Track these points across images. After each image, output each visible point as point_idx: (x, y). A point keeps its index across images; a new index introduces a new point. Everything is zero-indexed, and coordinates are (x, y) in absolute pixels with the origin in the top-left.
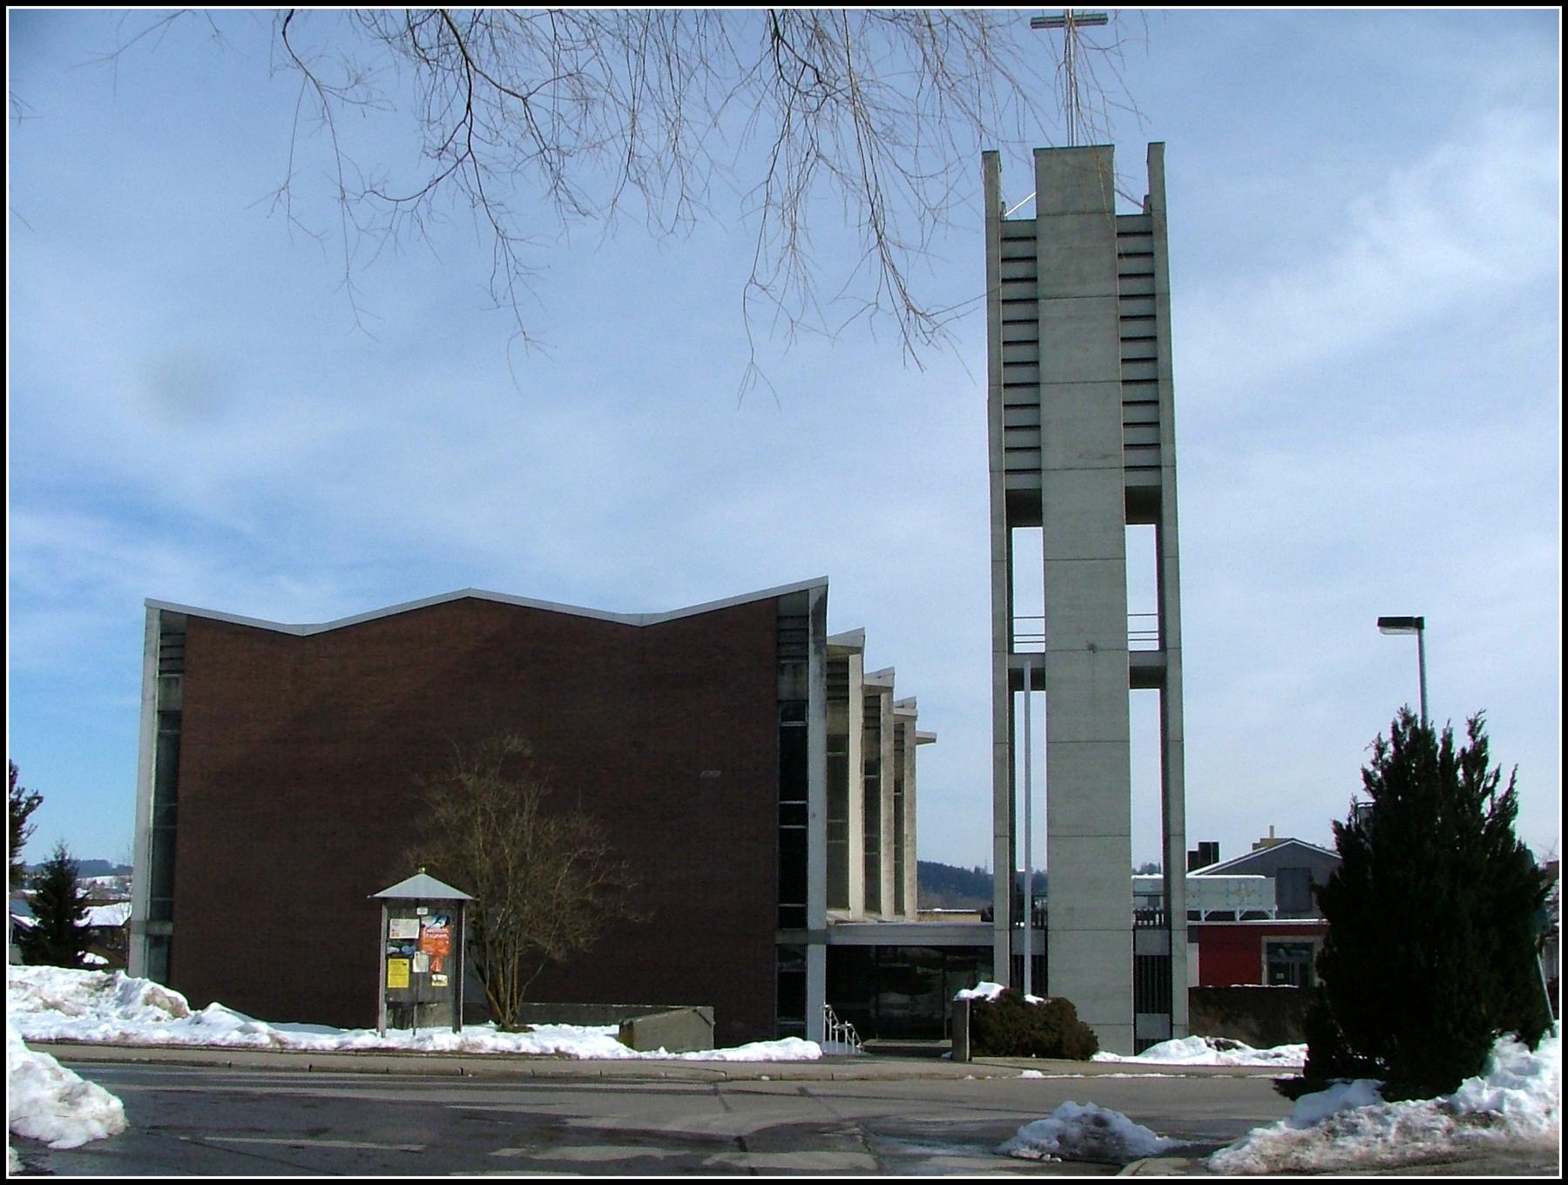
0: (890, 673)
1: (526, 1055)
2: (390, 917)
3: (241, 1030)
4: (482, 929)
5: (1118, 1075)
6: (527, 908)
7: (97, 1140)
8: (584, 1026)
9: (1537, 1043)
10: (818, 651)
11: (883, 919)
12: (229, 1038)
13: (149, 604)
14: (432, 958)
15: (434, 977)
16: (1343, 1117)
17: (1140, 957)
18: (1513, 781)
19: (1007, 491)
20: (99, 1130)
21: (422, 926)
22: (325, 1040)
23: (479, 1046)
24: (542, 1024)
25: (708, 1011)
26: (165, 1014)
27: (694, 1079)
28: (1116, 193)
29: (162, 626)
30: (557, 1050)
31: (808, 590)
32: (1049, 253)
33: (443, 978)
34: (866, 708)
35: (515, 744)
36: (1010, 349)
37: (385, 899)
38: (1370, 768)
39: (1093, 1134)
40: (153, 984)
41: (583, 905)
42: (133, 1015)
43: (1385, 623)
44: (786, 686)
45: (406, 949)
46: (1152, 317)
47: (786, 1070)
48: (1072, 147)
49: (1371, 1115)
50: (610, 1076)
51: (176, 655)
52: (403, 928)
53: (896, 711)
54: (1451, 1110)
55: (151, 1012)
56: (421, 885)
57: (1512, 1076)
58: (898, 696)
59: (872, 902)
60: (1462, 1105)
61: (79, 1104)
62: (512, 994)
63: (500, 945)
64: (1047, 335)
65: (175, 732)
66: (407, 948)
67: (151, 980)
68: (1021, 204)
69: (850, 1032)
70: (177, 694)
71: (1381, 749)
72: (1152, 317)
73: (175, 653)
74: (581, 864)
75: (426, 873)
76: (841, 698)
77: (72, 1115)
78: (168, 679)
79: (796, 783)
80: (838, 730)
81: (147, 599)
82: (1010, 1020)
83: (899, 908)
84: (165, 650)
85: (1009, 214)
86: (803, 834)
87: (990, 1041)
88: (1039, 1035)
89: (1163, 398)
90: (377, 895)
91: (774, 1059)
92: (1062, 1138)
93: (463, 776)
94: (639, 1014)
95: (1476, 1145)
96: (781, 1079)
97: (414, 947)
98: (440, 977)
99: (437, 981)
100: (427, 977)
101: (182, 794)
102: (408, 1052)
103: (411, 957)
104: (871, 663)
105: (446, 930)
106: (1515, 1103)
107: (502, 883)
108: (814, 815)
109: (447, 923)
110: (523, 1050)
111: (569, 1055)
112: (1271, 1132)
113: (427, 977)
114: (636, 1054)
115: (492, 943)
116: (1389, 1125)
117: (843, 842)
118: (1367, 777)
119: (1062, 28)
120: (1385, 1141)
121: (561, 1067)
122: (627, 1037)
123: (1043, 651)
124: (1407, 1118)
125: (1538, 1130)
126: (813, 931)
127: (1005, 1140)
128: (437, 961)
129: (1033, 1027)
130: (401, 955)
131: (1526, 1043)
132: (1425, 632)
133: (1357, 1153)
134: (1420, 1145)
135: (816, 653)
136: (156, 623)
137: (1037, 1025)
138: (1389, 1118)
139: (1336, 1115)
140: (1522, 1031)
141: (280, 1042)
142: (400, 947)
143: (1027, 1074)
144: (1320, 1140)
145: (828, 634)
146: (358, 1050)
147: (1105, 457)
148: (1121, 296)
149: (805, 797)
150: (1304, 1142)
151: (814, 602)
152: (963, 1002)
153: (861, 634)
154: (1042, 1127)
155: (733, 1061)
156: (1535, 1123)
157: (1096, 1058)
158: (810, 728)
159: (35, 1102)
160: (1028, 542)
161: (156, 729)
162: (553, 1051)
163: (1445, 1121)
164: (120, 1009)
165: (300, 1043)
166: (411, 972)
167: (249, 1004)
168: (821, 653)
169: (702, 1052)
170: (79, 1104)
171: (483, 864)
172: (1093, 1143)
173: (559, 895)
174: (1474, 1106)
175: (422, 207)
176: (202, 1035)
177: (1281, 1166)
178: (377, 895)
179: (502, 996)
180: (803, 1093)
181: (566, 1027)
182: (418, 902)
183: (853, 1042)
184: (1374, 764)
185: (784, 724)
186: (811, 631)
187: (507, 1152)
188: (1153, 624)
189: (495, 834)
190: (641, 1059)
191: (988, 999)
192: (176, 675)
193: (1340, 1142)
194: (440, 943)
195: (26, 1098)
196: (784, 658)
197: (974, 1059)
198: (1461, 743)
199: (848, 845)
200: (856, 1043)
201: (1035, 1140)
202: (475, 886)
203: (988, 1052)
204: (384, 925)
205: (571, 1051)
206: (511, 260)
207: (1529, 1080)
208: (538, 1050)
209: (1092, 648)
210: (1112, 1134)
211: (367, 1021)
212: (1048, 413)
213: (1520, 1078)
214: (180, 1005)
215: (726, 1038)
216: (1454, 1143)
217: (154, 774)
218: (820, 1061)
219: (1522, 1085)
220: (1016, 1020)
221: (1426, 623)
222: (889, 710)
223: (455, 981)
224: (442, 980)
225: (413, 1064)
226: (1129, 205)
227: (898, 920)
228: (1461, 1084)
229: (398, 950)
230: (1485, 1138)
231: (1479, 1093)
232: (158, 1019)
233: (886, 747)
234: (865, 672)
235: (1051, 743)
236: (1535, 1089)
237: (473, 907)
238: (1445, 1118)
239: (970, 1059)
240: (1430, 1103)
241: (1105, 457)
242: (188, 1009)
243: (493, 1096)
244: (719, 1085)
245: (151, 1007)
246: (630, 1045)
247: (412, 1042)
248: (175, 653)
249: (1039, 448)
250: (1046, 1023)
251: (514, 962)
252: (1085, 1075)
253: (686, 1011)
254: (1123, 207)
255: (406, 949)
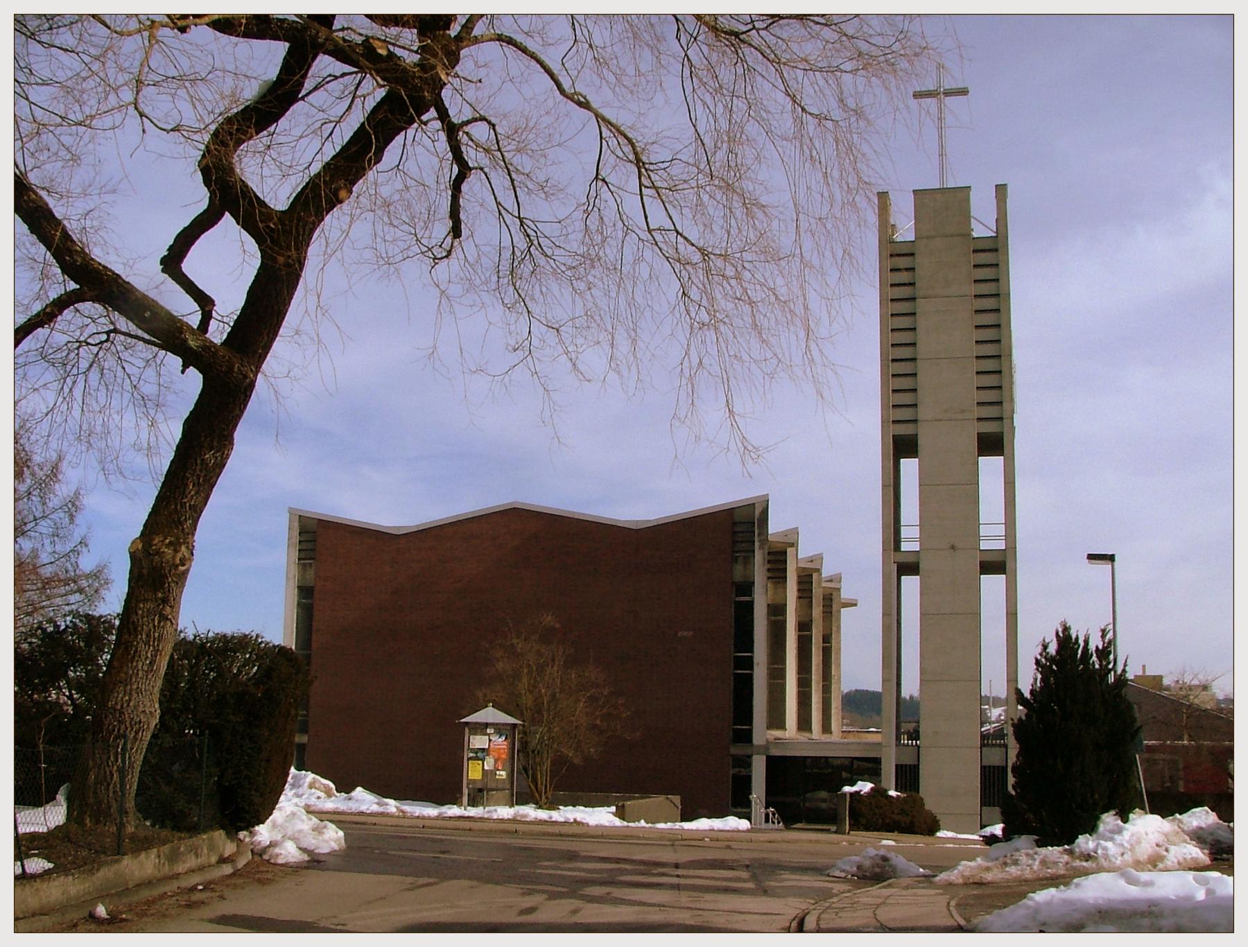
0: (820, 558)
1: (556, 823)
2: (470, 734)
3: (378, 804)
4: (527, 742)
5: (949, 845)
6: (555, 730)
7: (335, 851)
8: (593, 807)
9: (1128, 817)
10: (761, 547)
11: (813, 738)
12: (371, 808)
13: (292, 511)
14: (496, 761)
15: (498, 772)
16: (1012, 856)
17: (985, 767)
18: (1125, 665)
19: (893, 436)
20: (335, 846)
21: (490, 740)
22: (431, 811)
23: (526, 816)
24: (565, 806)
25: (677, 799)
26: (322, 795)
27: (661, 838)
28: (972, 220)
29: (300, 526)
30: (575, 820)
31: (754, 504)
32: (924, 265)
33: (503, 773)
34: (799, 583)
35: (549, 619)
36: (896, 334)
37: (467, 723)
38: (1039, 657)
39: (878, 866)
40: (314, 775)
41: (595, 727)
42: (302, 795)
43: (1091, 557)
44: (738, 572)
45: (480, 754)
46: (998, 311)
47: (721, 835)
48: (944, 188)
49: (1027, 855)
50: (607, 835)
51: (310, 547)
52: (478, 742)
53: (824, 585)
54: (1070, 852)
55: (314, 793)
56: (489, 714)
57: (1108, 834)
58: (826, 573)
59: (804, 723)
60: (1077, 850)
61: (323, 833)
62: (546, 786)
63: (538, 753)
64: (922, 323)
65: (309, 601)
66: (481, 754)
67: (313, 773)
68: (905, 231)
69: (774, 814)
70: (311, 574)
71: (1045, 647)
72: (998, 311)
73: (310, 546)
74: (593, 699)
75: (493, 706)
76: (782, 578)
77: (321, 838)
78: (304, 565)
79: (744, 639)
80: (779, 601)
81: (290, 508)
82: (877, 807)
83: (826, 728)
84: (303, 543)
85: (898, 237)
86: (750, 677)
87: (863, 821)
88: (897, 817)
89: (1005, 370)
90: (462, 720)
91: (716, 829)
92: (859, 867)
93: (515, 641)
94: (630, 799)
95: (1079, 870)
96: (717, 840)
97: (485, 754)
98: (502, 773)
99: (500, 775)
100: (493, 772)
101: (314, 645)
102: (481, 819)
103: (483, 760)
104: (805, 550)
105: (505, 743)
106: (1105, 849)
107: (539, 712)
108: (758, 664)
109: (506, 738)
110: (553, 819)
111: (583, 823)
112: (973, 864)
113: (493, 772)
114: (625, 823)
115: (533, 752)
116: (1035, 860)
117: (807, 676)
118: (1038, 662)
119: (946, 87)
120: (1031, 869)
121: (577, 830)
122: (621, 814)
123: (918, 549)
124: (1046, 856)
125: (1115, 863)
126: (758, 746)
127: (827, 869)
128: (499, 763)
129: (893, 813)
130: (477, 758)
131: (1120, 816)
132: (1116, 563)
133: (1014, 875)
134: (1049, 871)
135: (760, 549)
136: (296, 524)
137: (896, 811)
138: (1036, 856)
139: (1009, 855)
140: (1120, 810)
141: (403, 811)
142: (476, 753)
143: (885, 842)
144: (997, 868)
145: (770, 532)
146: (450, 817)
147: (963, 411)
148: (975, 296)
149: (752, 651)
150: (988, 869)
151: (761, 510)
152: (845, 794)
153: (795, 531)
154: (849, 861)
155: (688, 830)
156: (1113, 860)
157: (939, 834)
158: (755, 601)
159: (300, 831)
160: (909, 467)
161: (296, 599)
162: (572, 820)
163: (1066, 858)
164: (293, 791)
165: (415, 812)
166: (483, 769)
167: (381, 789)
168: (763, 548)
169: (669, 824)
170: (323, 833)
171: (527, 700)
172: (878, 870)
173: (577, 721)
174: (1084, 850)
175: (507, 379)
176: (352, 806)
177: (971, 881)
178: (462, 720)
179: (539, 785)
180: (729, 847)
181: (582, 808)
182: (487, 725)
183: (776, 822)
184: (1041, 655)
185: (737, 599)
186: (756, 532)
187: (546, 863)
188: (1001, 530)
189: (535, 680)
190: (628, 827)
191: (862, 793)
192: (310, 561)
193: (1007, 869)
194: (502, 751)
195: (296, 829)
196: (737, 552)
197: (851, 832)
198: (1096, 642)
199: (784, 684)
200: (779, 823)
201: (844, 868)
202: (522, 714)
203: (862, 828)
204: (466, 739)
205: (584, 821)
206: (551, 404)
207: (1116, 836)
208: (563, 820)
209: (953, 547)
210: (891, 866)
211: (455, 800)
212: (923, 380)
213: (1112, 835)
214: (331, 789)
215: (687, 816)
216: (1067, 870)
217: (295, 630)
218: (748, 831)
219: (1111, 839)
220: (881, 807)
221: (1116, 558)
222: (820, 583)
223: (511, 775)
224: (503, 774)
225: (486, 826)
226: (982, 227)
227: (825, 738)
228: (1077, 838)
229: (474, 755)
230: (1084, 867)
231: (1087, 843)
232: (319, 798)
233: (817, 611)
234: (799, 557)
235: (924, 615)
236: (1118, 841)
237: (521, 728)
238: (1066, 857)
239: (849, 833)
240: (1060, 849)
241: (963, 411)
242: (335, 792)
243: (537, 842)
244: (675, 841)
245: (313, 790)
246: (622, 817)
247: (484, 813)
248: (310, 546)
249: (915, 405)
250: (902, 810)
251: (547, 765)
252: (926, 844)
253: (662, 798)
254: (979, 231)
255: (480, 754)
